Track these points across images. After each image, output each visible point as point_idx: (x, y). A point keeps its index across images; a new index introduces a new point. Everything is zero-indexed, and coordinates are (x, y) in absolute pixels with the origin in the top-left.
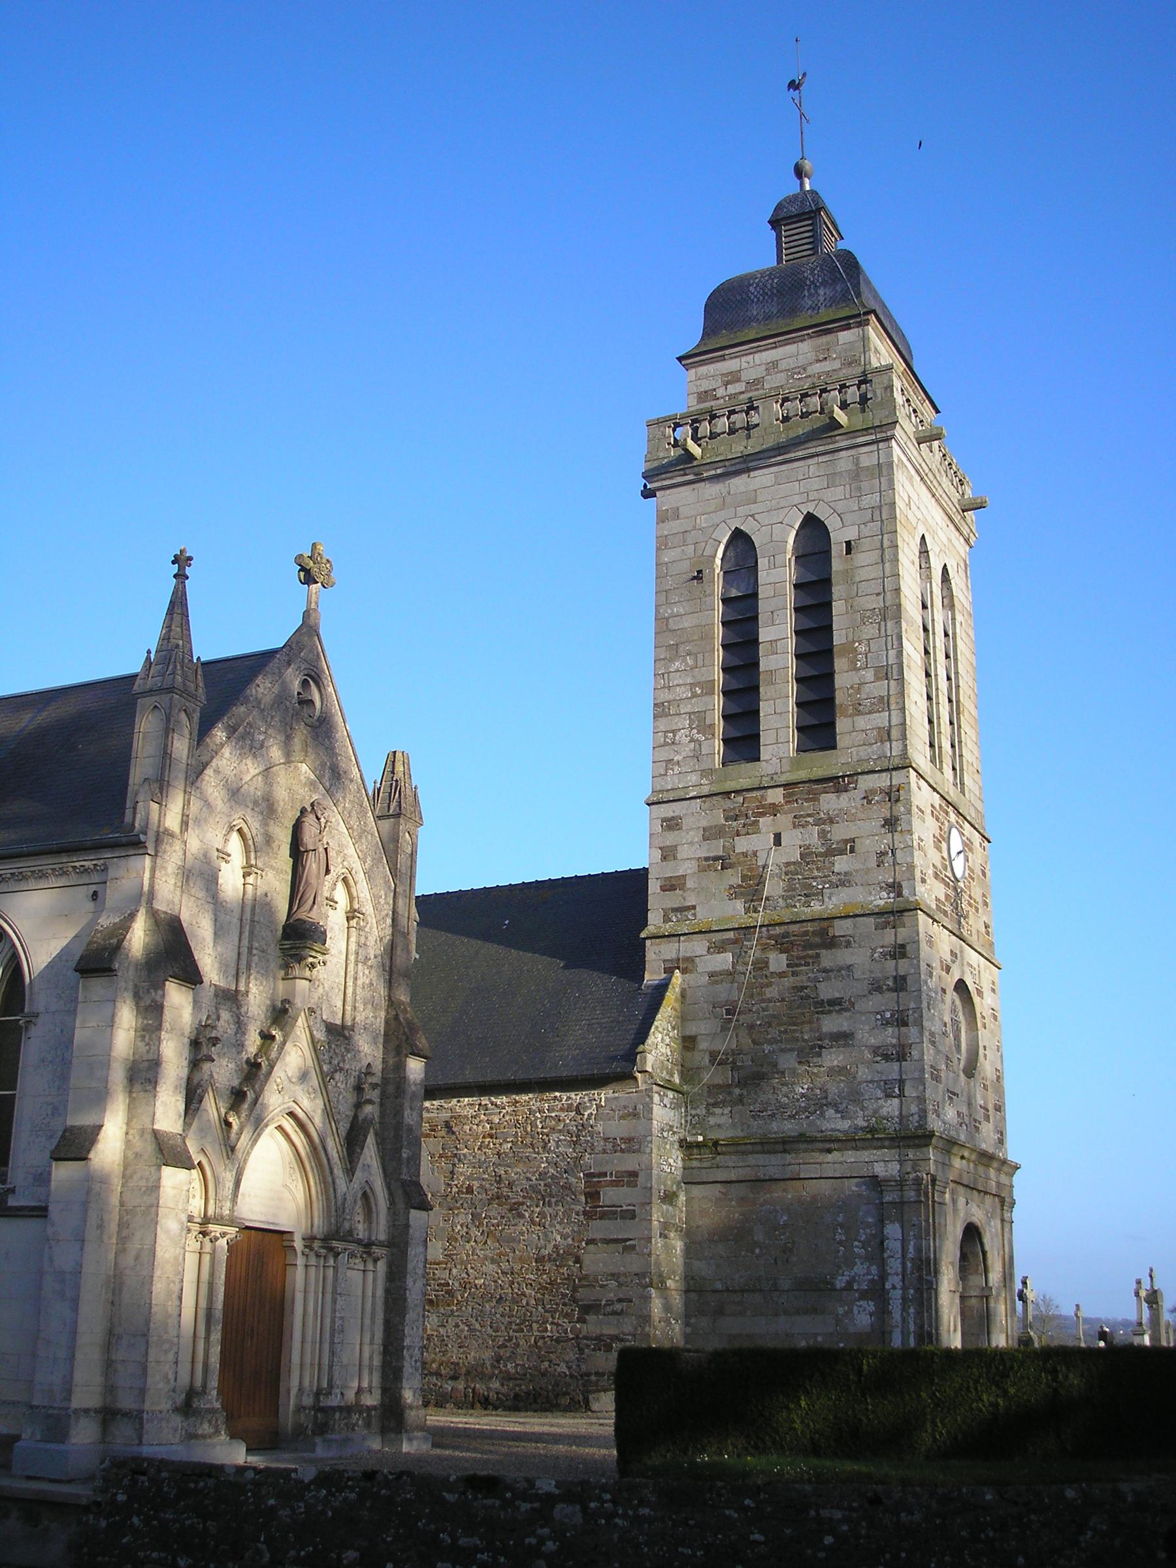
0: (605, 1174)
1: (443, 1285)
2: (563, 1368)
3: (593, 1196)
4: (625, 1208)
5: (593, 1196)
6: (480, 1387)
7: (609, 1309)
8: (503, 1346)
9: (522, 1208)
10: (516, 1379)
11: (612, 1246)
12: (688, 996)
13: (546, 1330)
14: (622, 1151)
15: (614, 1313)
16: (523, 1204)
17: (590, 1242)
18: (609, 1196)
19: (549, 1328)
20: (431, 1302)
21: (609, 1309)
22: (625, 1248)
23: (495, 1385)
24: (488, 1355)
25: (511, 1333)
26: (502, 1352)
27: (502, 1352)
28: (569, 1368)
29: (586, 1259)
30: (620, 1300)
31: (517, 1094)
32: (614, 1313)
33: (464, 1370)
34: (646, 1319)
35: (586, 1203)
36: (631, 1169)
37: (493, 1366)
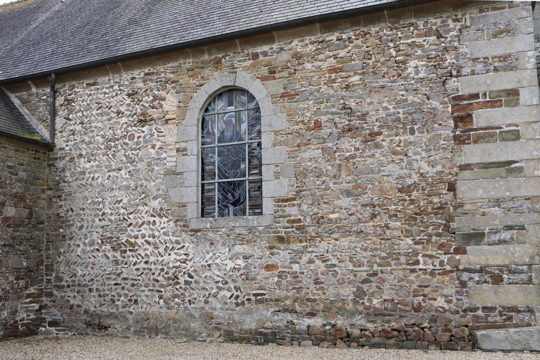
0: (476, 96)
1: (294, 221)
2: (440, 302)
3: (463, 118)
4: (506, 129)
5: (463, 118)
6: (340, 322)
7: (495, 238)
8: (364, 282)
9: (379, 138)
10: (384, 315)
11: (493, 171)
12: (400, 232)
13: (417, 262)
14: (496, 69)
15: (501, 242)
16: (380, 134)
17: (463, 168)
18: (482, 117)
19: (421, 260)
20: (281, 239)
21: (495, 238)
22: (511, 171)
23: (360, 321)
24: (348, 292)
25: (375, 267)
26: (365, 287)
27: (365, 287)
28: (449, 302)
29: (461, 187)
30: (509, 228)
31: (365, 26)
32: (501, 242)
33: (321, 307)
34: (27, 108)
35: (456, 126)
36: (509, 86)
37: (355, 302)
